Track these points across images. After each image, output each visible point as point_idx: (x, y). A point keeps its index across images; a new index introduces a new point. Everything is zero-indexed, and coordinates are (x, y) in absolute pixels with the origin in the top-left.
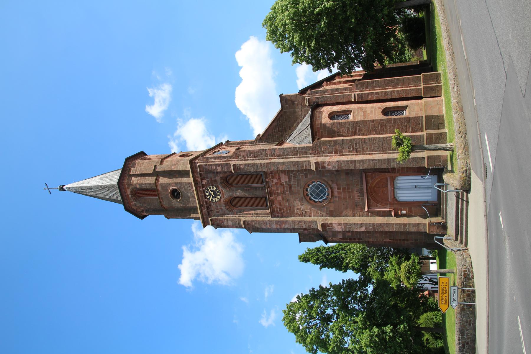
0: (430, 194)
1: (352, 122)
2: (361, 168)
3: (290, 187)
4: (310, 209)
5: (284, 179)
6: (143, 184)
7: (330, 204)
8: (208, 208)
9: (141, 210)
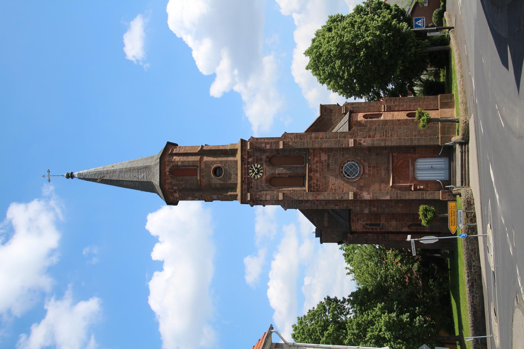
0: (443, 175)
1: (383, 121)
2: (390, 145)
3: (328, 165)
4: (343, 184)
6: (186, 161)
7: (360, 181)
8: (248, 184)
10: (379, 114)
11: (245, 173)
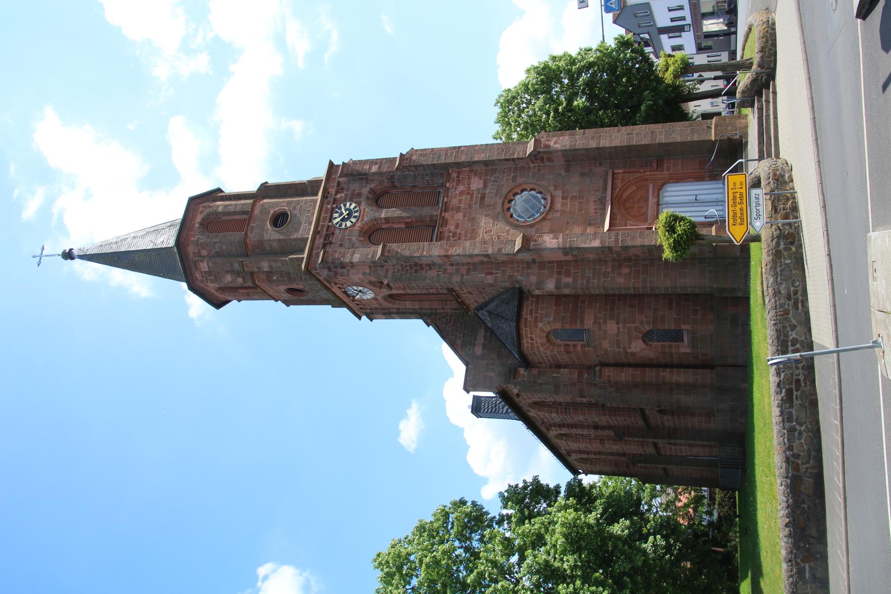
3: (483, 198)
4: (508, 232)
7: (544, 223)
8: (327, 237)
11: (325, 218)
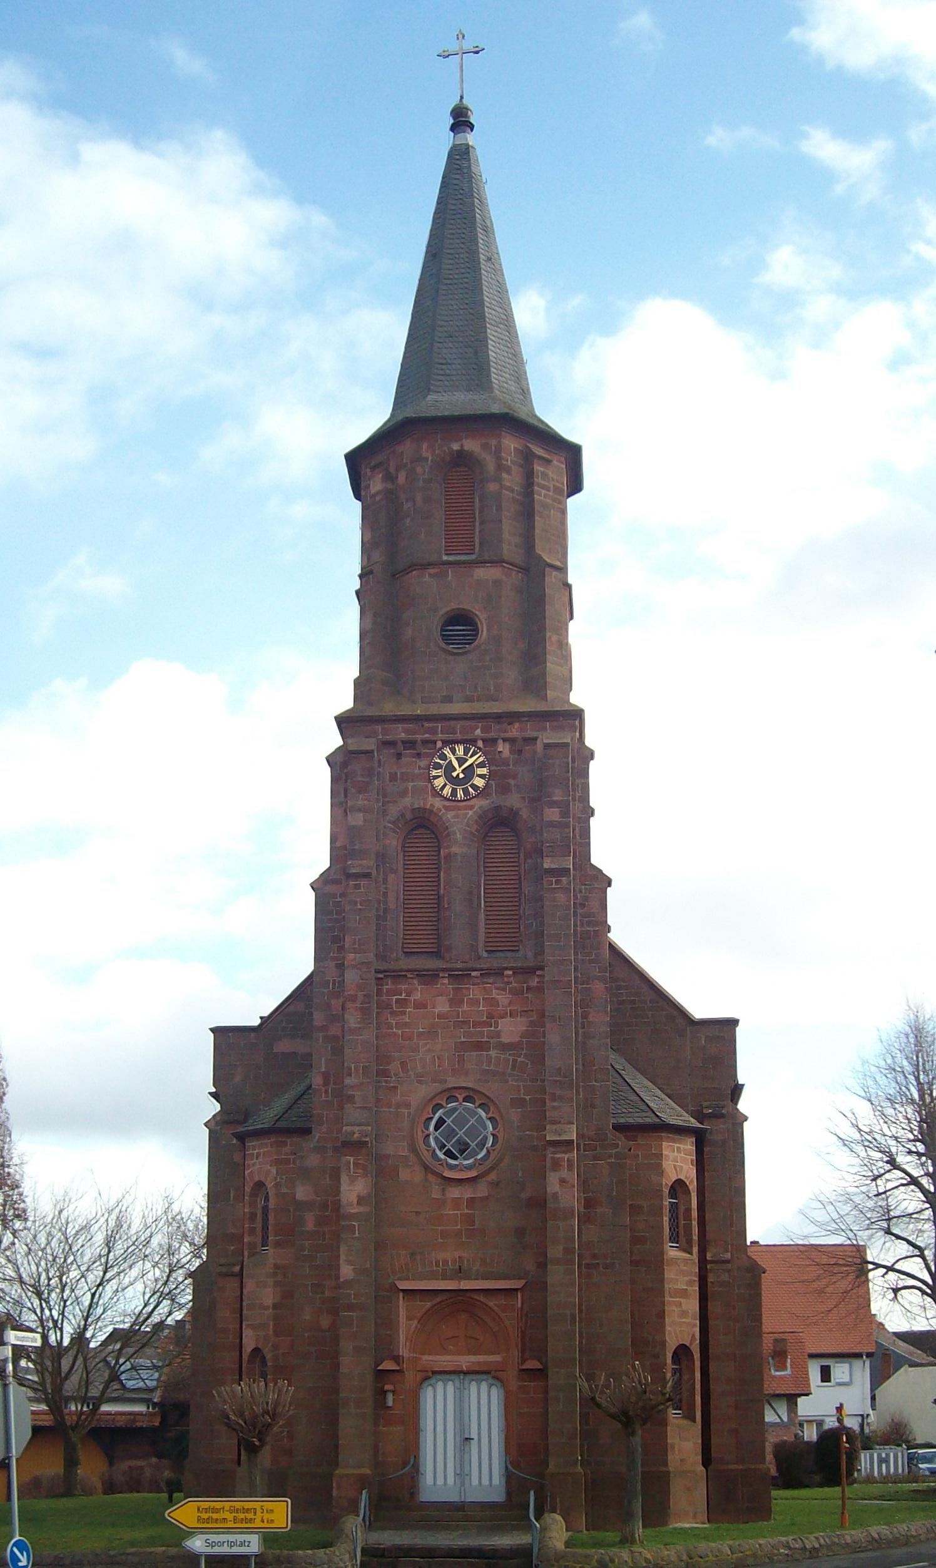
0: (440, 1482)
1: (662, 1253)
3: (480, 1046)
5: (511, 1029)
8: (410, 744)
9: (392, 470)
10: (689, 1241)
